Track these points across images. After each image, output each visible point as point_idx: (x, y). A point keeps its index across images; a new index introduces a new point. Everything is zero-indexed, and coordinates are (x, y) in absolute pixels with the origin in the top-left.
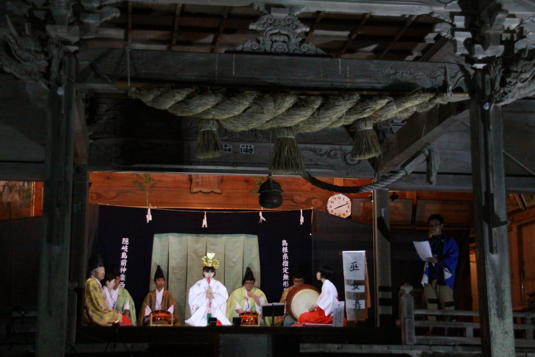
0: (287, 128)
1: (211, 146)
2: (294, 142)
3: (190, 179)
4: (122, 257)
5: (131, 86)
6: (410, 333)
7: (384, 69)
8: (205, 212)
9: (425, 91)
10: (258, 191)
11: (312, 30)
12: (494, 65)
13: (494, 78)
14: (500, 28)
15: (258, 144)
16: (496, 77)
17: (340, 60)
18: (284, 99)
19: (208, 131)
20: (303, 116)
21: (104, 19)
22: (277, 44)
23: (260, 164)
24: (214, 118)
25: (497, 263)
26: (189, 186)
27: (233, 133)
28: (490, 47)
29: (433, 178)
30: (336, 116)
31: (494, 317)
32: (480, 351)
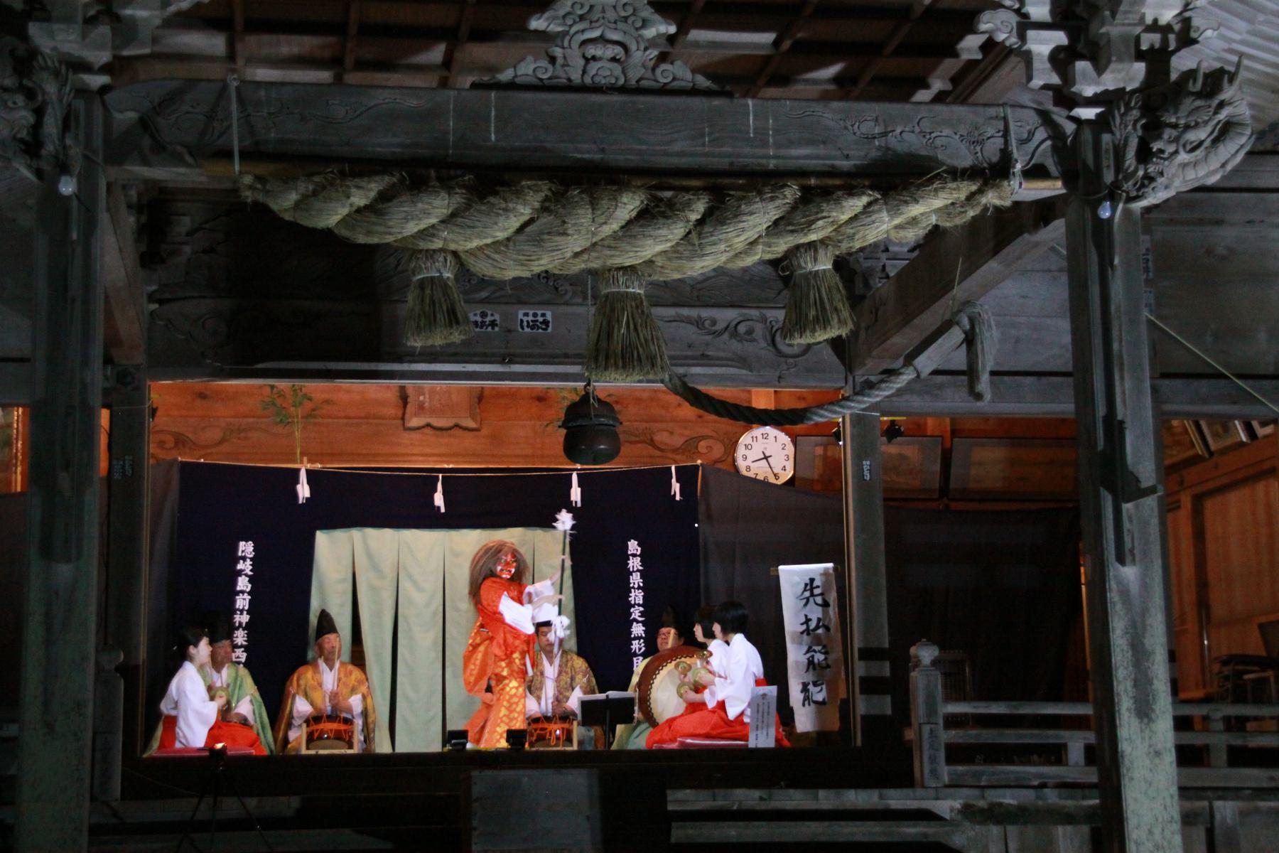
0: (624, 269)
1: (439, 316)
2: (642, 302)
3: (404, 398)
4: (238, 588)
5: (241, 172)
6: (933, 760)
7: (857, 124)
8: (440, 475)
9: (957, 174)
10: (560, 423)
11: (683, 30)
12: (1122, 110)
13: (1122, 142)
14: (1136, 22)
15: (562, 309)
16: (1126, 139)
17: (750, 102)
18: (615, 199)
19: (432, 278)
20: (664, 239)
21: (173, 9)
22: (599, 64)
23: (566, 358)
24: (445, 247)
25: (1135, 589)
26: (400, 414)
27: (499, 285)
28: (1113, 66)
29: (984, 383)
30: (742, 238)
31: (1129, 717)
32: (1095, 798)
